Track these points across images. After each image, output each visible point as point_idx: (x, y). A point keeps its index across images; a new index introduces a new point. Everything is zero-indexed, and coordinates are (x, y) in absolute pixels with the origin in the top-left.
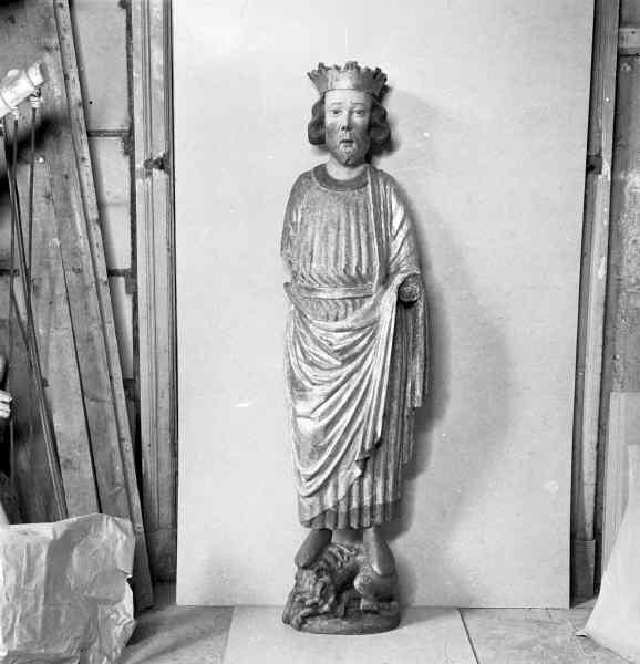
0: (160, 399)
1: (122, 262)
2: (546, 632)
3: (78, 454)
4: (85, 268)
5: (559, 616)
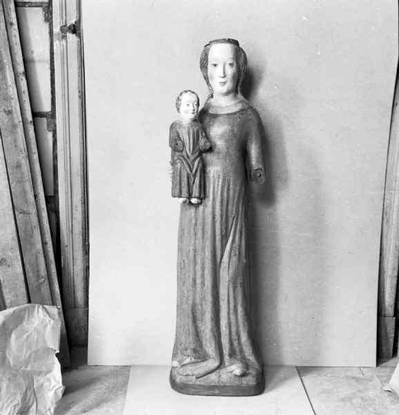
0: (74, 211)
1: (46, 107)
2: (361, 387)
3: (11, 254)
4: (13, 109)
5: (370, 374)
